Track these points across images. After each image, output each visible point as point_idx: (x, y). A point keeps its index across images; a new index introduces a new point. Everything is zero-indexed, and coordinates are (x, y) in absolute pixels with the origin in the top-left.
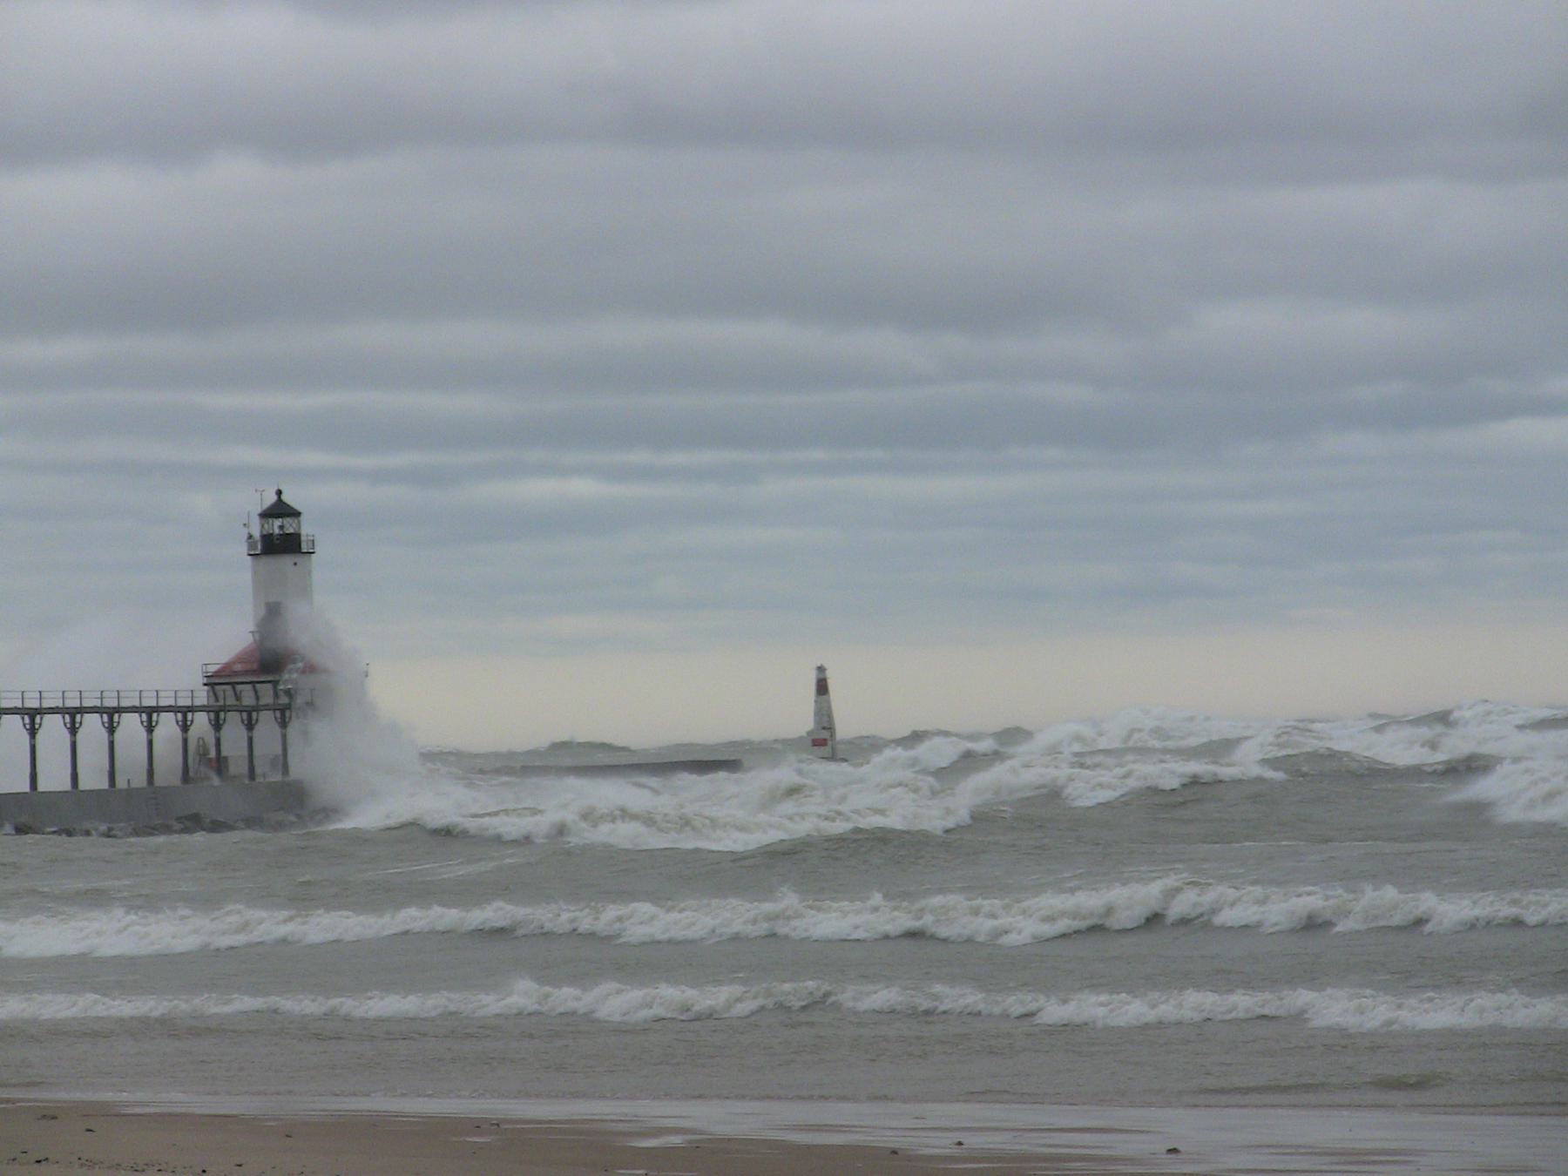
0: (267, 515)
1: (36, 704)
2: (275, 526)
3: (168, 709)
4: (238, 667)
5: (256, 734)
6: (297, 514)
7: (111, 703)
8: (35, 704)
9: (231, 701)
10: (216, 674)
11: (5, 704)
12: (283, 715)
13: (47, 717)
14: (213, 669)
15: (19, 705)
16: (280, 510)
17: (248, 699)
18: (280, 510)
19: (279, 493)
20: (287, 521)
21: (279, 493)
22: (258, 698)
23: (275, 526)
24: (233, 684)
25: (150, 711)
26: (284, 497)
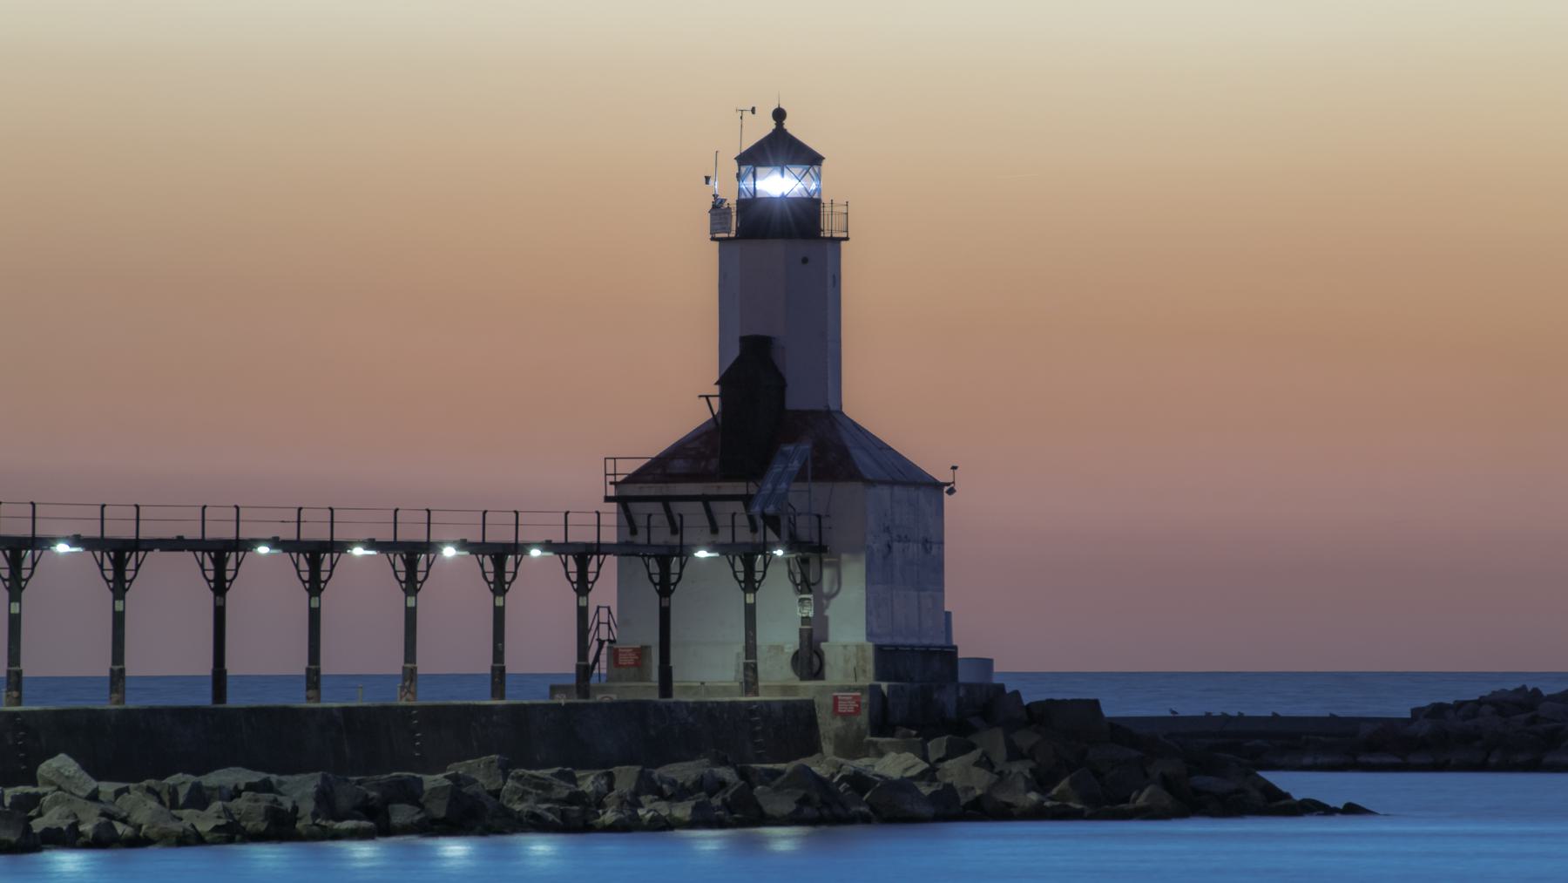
1: (129, 533)
2: (777, 184)
4: (679, 465)
8: (126, 532)
10: (633, 478)
14: (631, 467)
19: (779, 115)
21: (779, 115)
24: (666, 500)
26: (788, 125)
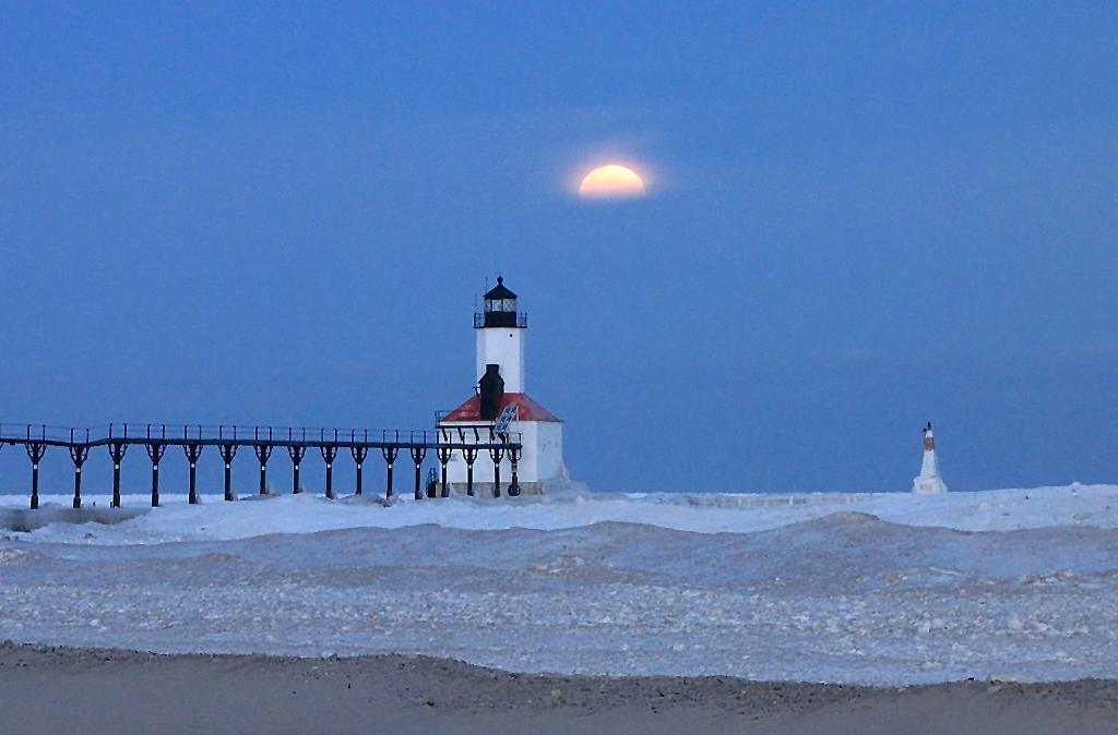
0: (490, 296)
1: (473, 442)
2: (496, 305)
3: (405, 446)
5: (364, 466)
6: (514, 297)
7: (359, 439)
9: (456, 440)
11: (7, 433)
12: (79, 453)
13: (130, 446)
15: (218, 438)
16: (500, 292)
17: (470, 440)
18: (500, 292)
19: (500, 280)
20: (506, 302)
21: (500, 280)
22: (478, 439)
23: (496, 305)
25: (229, 444)
